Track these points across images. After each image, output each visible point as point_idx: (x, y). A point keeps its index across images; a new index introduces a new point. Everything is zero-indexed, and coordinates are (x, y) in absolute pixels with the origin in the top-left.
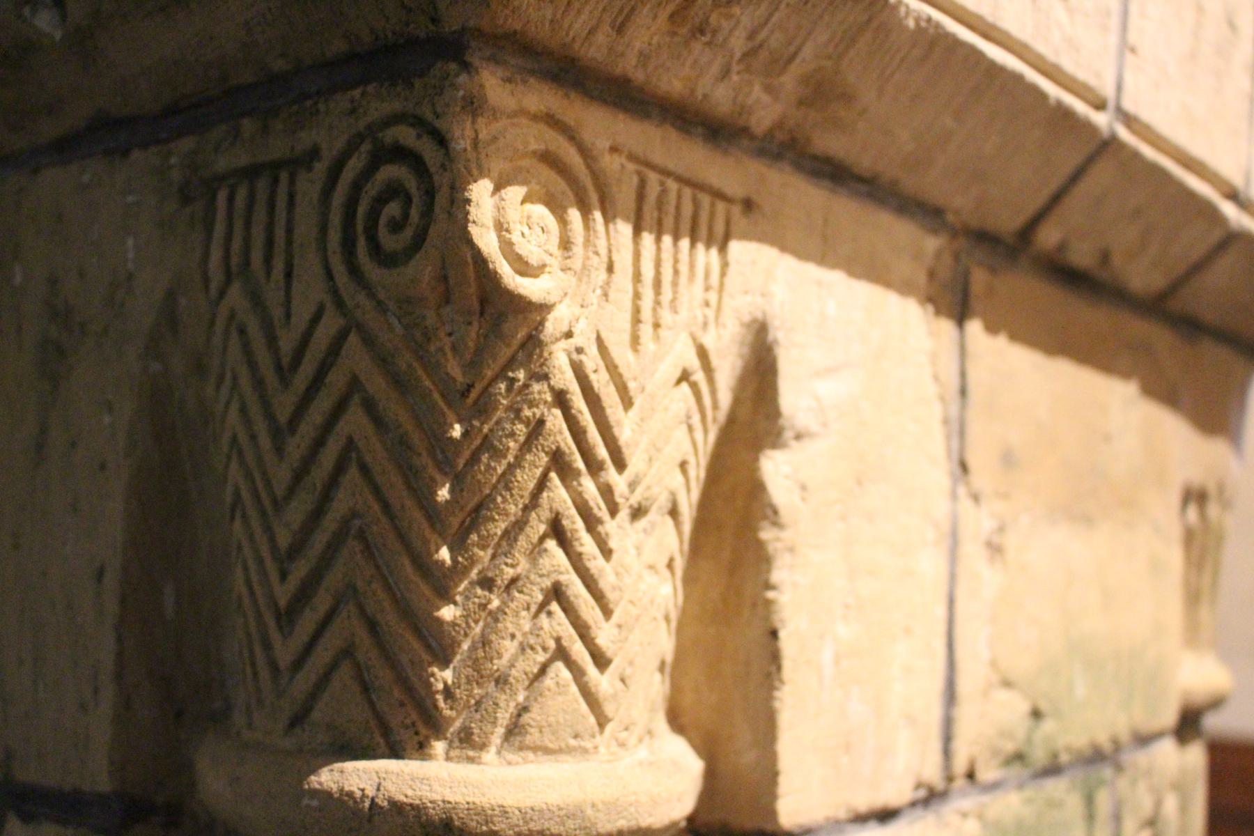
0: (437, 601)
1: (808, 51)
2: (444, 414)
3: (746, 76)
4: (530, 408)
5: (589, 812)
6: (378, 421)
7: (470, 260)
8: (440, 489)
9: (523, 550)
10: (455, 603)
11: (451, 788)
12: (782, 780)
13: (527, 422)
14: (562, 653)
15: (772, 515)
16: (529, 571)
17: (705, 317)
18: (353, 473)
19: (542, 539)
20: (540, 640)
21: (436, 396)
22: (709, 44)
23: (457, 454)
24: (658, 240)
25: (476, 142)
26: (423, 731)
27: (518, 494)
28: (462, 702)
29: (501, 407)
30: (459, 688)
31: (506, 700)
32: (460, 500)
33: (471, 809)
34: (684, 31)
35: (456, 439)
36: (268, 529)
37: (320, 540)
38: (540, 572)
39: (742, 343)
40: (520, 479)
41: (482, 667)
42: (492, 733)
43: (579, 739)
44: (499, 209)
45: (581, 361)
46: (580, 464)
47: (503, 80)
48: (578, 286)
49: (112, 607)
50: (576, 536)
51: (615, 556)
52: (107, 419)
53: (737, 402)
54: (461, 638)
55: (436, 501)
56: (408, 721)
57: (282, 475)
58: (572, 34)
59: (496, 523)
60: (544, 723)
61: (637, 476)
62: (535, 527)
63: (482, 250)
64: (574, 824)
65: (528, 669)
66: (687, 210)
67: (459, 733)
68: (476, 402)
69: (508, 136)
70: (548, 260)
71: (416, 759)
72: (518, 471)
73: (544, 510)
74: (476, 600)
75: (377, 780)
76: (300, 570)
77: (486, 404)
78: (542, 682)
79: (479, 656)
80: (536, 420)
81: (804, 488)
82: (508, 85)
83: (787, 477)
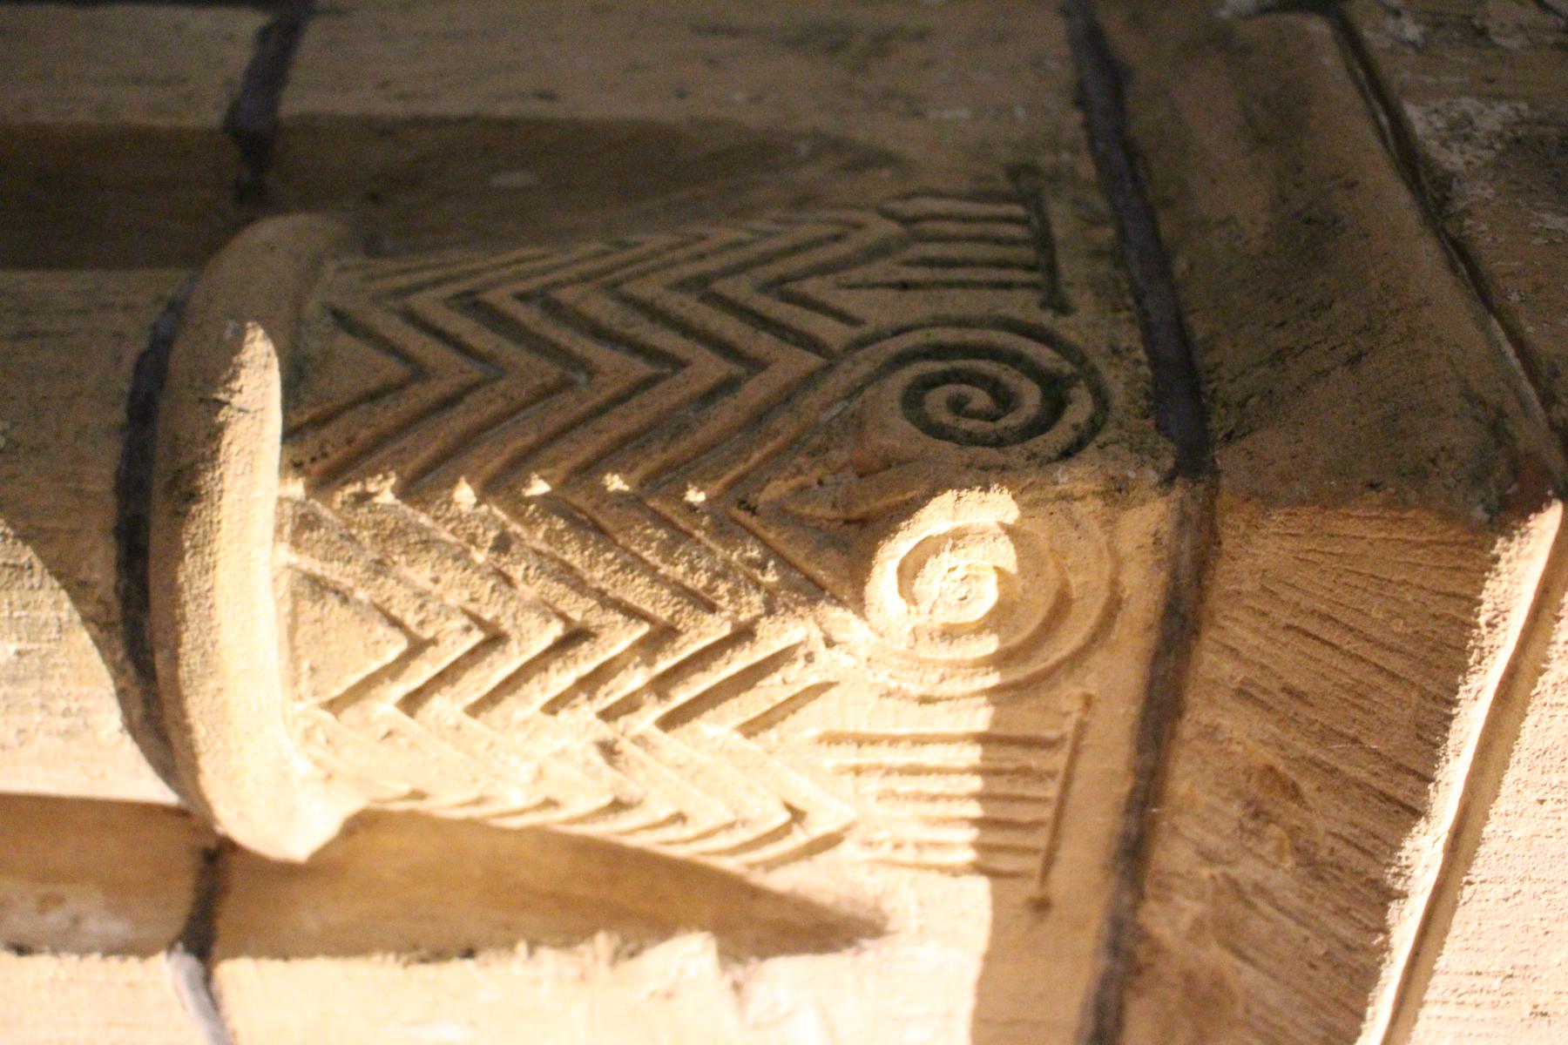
0: (479, 481)
1: (1250, 976)
2: (717, 477)
3: (1209, 893)
4: (729, 591)
5: (212, 684)
6: (709, 397)
7: (909, 495)
8: (621, 478)
9: (546, 590)
10: (478, 504)
11: (240, 500)
12: (278, 966)
13: (710, 589)
14: (417, 647)
15: (629, 951)
16: (520, 600)
17: (880, 843)
18: (642, 369)
19: (562, 616)
20: (432, 617)
21: (740, 468)
22: (1242, 827)
23: (666, 498)
24: (975, 771)
25: (1066, 497)
26: (316, 468)
27: (617, 581)
28: (351, 516)
29: (728, 552)
30: (370, 512)
31: (355, 573)
32: (607, 504)
33: (211, 526)
34: (1254, 788)
35: (684, 496)
36: (584, 279)
37: (563, 336)
38: (519, 614)
39: (854, 902)
40: (637, 581)
41: (396, 540)
42: (313, 556)
43: (309, 673)
44: (982, 533)
45: (795, 660)
46: (664, 664)
47: (1156, 533)
48: (896, 654)
49: (504, 110)
50: (570, 663)
51: (549, 719)
52: (739, 96)
53: (779, 899)
54: (432, 512)
55: (604, 473)
56: (328, 449)
57: (646, 290)
58: (1227, 623)
59: (579, 552)
60: (327, 625)
61: (655, 747)
62: (577, 605)
63: (922, 510)
64: (195, 664)
65: (395, 602)
66: (1024, 813)
67: (314, 514)
68: (735, 521)
69: (1082, 542)
70: (924, 607)
71: (281, 459)
72: (647, 579)
73: (598, 616)
74: (480, 531)
75: (252, 409)
76: (528, 315)
77: (730, 532)
78: (380, 621)
79: (410, 536)
80: (713, 600)
81: (669, 995)
82: (1152, 540)
83: (681, 971)
